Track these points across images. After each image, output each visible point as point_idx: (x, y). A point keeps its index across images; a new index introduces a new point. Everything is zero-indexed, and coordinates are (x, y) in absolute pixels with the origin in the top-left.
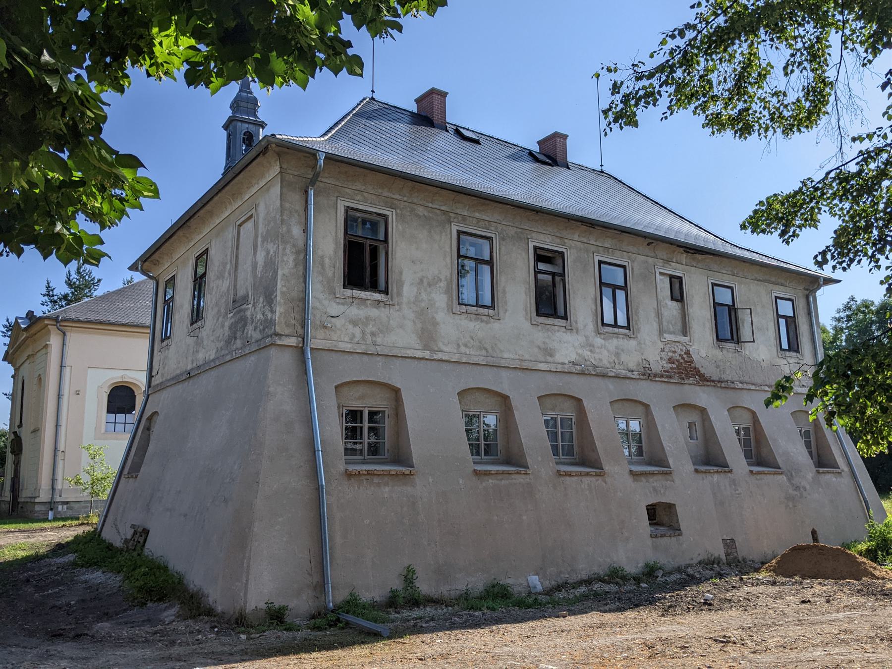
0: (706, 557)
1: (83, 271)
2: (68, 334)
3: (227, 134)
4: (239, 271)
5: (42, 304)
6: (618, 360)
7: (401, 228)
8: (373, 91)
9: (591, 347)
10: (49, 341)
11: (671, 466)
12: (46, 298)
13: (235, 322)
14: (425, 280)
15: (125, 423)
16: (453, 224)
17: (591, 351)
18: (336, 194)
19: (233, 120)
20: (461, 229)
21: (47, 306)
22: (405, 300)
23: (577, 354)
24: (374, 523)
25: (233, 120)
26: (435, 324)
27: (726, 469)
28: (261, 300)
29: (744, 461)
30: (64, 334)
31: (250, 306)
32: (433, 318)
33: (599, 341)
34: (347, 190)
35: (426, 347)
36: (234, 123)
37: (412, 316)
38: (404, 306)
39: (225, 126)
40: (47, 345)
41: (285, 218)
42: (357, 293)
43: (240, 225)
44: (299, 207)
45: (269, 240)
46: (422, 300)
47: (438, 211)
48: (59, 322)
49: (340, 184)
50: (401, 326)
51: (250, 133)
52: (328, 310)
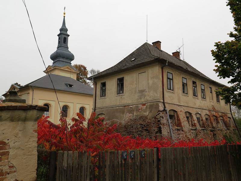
35: (179, 102)
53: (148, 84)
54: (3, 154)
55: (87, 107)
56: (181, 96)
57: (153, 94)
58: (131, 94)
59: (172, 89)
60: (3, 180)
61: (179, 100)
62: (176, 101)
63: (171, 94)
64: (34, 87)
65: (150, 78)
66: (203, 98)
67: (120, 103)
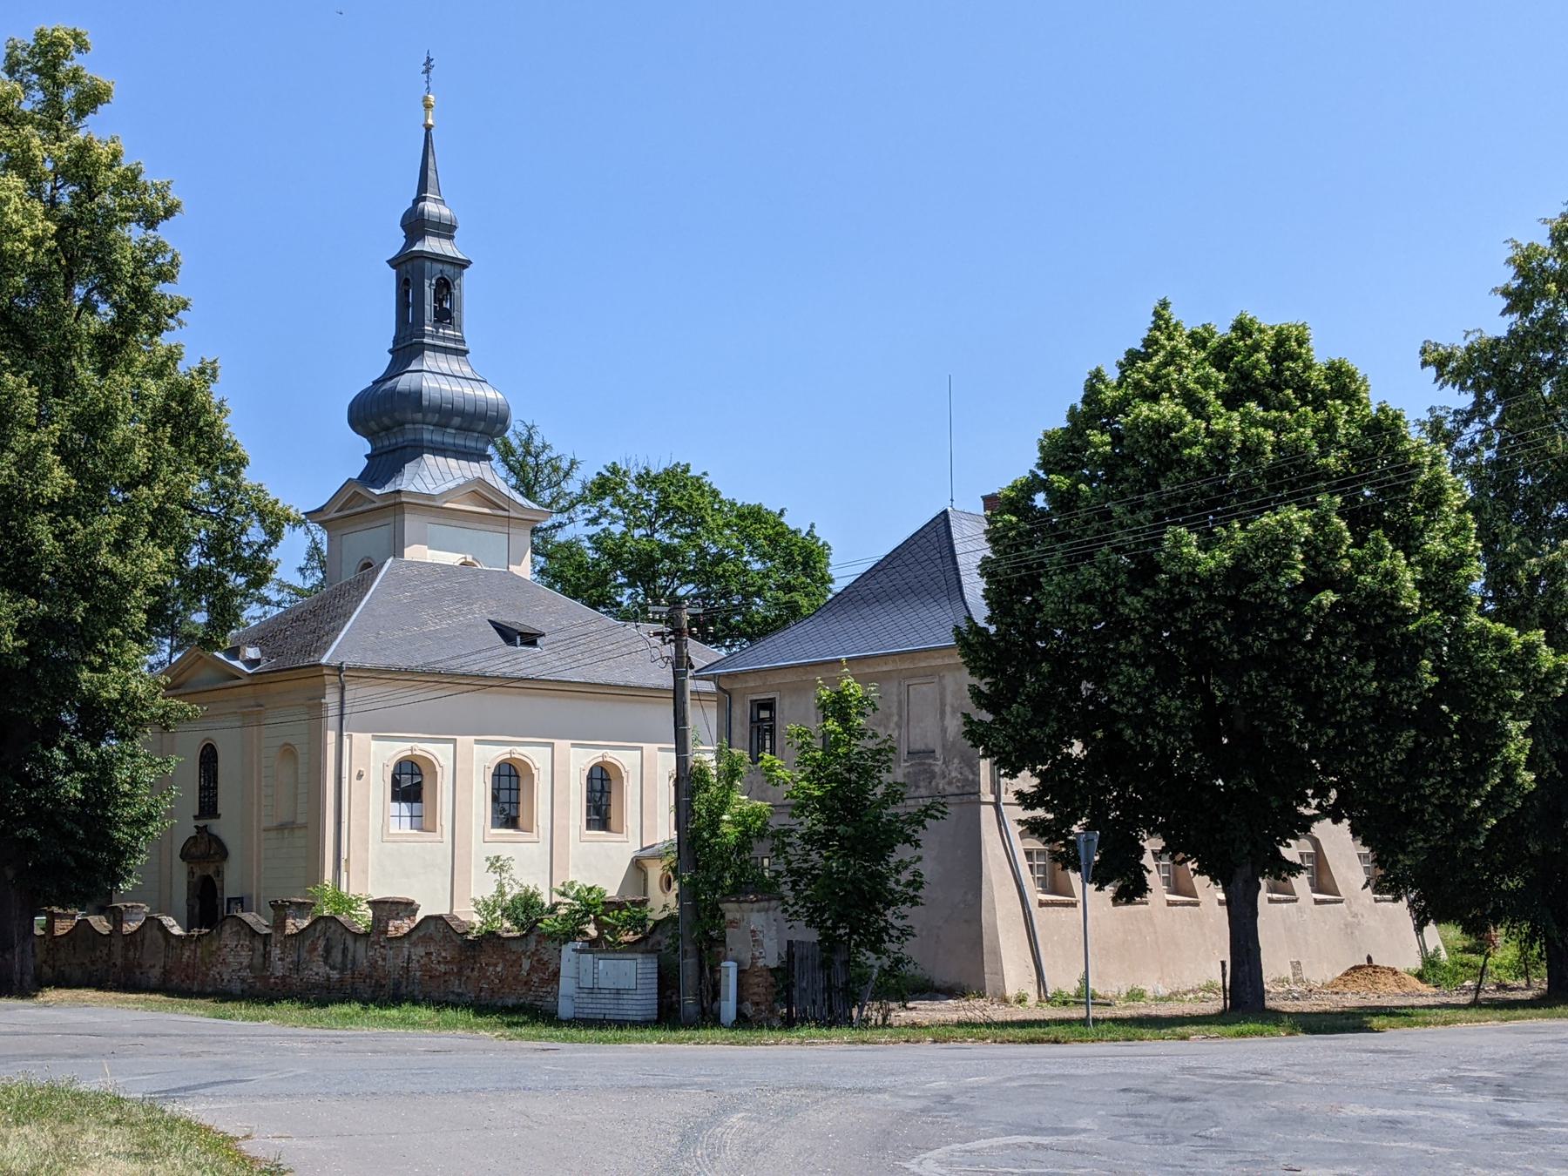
3: (398, 275)
28: (956, 761)
30: (343, 688)
53: (944, 730)
65: (948, 709)
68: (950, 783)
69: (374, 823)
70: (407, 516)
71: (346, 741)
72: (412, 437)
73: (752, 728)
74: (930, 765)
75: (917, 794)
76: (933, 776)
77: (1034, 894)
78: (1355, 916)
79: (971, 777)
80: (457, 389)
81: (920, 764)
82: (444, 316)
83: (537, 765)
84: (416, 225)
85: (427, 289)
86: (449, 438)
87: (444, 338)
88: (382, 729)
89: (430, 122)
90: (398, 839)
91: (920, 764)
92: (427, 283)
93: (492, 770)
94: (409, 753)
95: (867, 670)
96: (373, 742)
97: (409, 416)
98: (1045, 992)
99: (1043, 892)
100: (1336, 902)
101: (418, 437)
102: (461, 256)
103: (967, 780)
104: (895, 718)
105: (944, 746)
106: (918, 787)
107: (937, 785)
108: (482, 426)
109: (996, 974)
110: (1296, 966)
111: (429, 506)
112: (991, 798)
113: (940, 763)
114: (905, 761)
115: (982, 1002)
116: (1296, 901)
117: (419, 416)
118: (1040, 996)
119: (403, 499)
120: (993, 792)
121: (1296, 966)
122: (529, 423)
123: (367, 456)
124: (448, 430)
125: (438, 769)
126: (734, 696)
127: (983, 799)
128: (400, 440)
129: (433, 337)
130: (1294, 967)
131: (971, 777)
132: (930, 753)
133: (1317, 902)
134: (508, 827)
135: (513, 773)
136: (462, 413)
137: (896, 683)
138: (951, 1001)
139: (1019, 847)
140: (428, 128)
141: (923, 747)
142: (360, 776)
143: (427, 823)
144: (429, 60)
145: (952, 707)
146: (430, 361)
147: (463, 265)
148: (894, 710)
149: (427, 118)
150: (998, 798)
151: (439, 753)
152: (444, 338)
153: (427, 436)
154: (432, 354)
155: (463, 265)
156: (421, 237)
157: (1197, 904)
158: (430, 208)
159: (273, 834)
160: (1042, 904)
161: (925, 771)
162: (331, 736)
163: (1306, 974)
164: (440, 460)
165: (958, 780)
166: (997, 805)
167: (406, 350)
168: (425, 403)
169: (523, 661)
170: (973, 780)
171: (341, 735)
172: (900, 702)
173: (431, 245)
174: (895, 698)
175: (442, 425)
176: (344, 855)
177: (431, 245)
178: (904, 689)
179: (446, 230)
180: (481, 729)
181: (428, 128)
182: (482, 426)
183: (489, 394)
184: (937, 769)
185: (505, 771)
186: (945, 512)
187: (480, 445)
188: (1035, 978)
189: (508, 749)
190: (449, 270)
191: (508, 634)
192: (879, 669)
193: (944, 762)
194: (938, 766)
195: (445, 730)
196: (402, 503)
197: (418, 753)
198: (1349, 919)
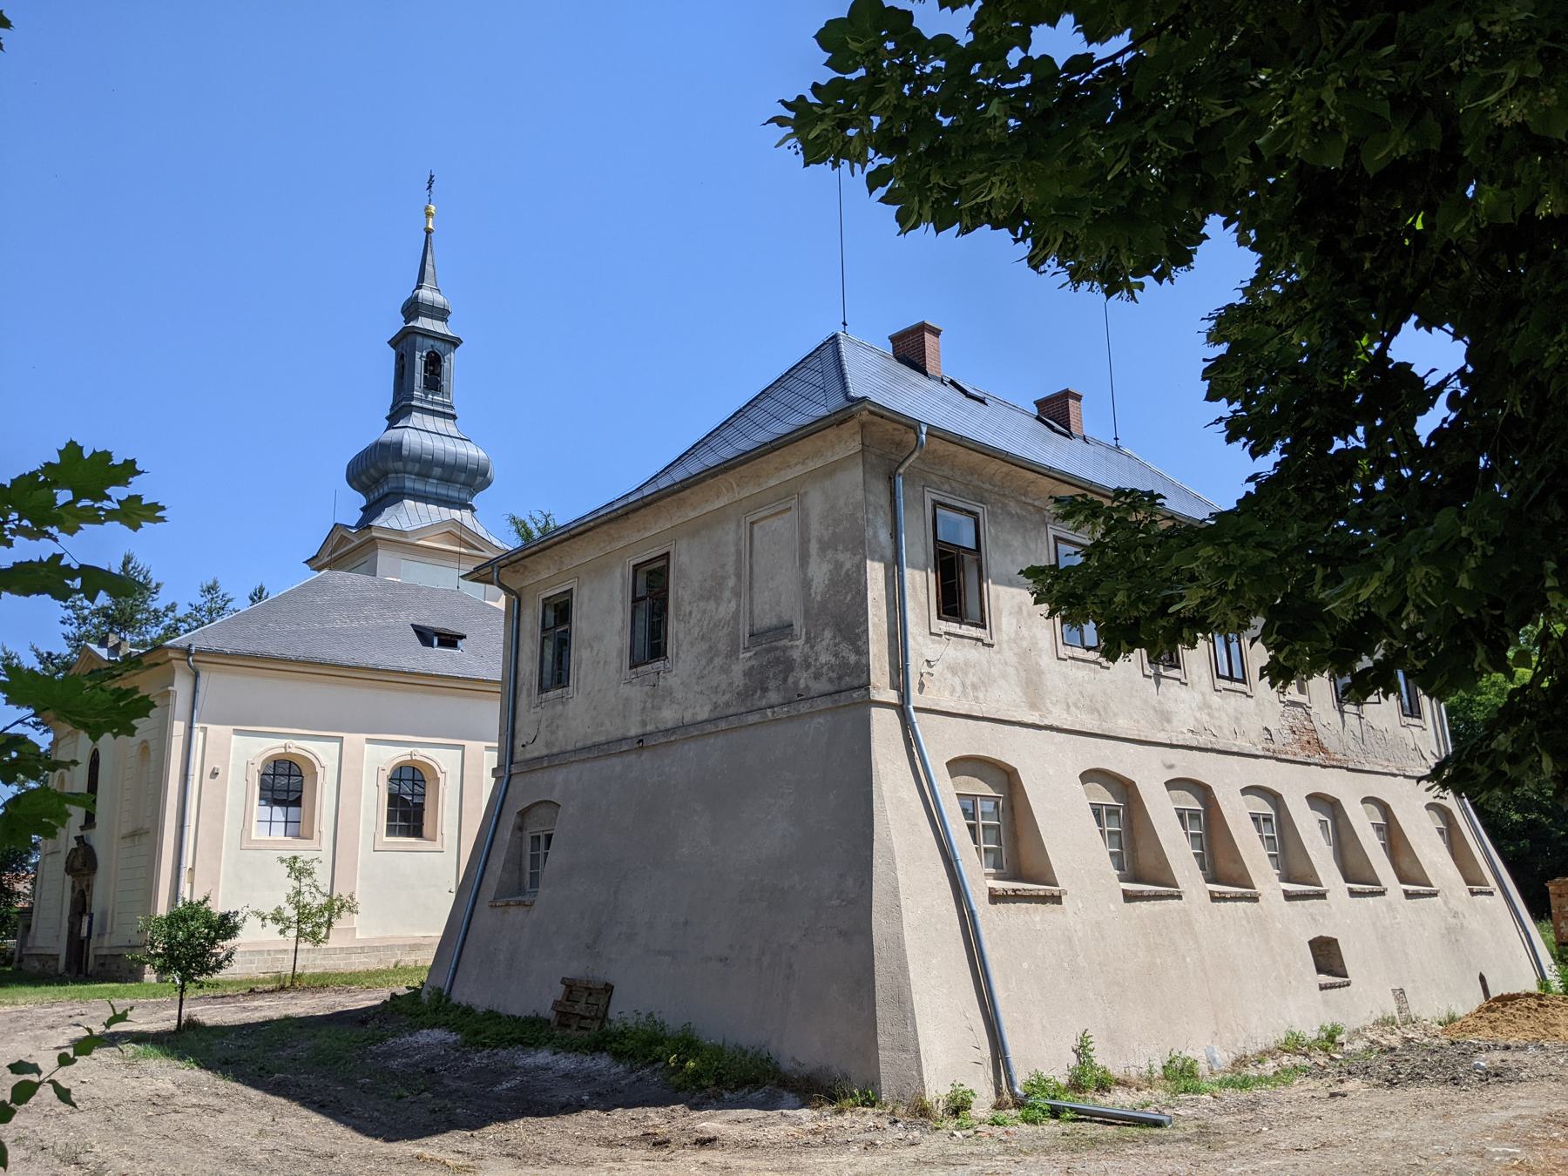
0: (1380, 1017)
1: (133, 568)
2: (202, 674)
3: (397, 354)
4: (755, 590)
5: (62, 622)
6: (1239, 727)
7: (993, 531)
8: (845, 324)
9: (1206, 706)
10: (173, 685)
11: (1323, 883)
12: (70, 612)
13: (761, 666)
14: (1024, 608)
15: (271, 821)
16: (1049, 526)
17: (1209, 715)
18: (922, 484)
19: (409, 333)
20: (1058, 534)
21: (71, 625)
22: (1005, 638)
23: (1196, 719)
24: (1033, 967)
25: (409, 333)
26: (1040, 673)
27: (1376, 888)
28: (828, 634)
29: (1274, 873)
30: (196, 676)
31: (800, 643)
32: (1037, 663)
33: (1216, 699)
34: (933, 477)
35: (1033, 706)
36: (410, 338)
37: (1013, 660)
38: (1005, 646)
39: (393, 343)
40: (169, 692)
41: (870, 516)
42: (953, 627)
43: (752, 523)
44: (884, 500)
45: (841, 548)
46: (1023, 638)
47: (1030, 508)
48: (191, 655)
49: (926, 469)
50: (1004, 676)
51: (436, 354)
52: (924, 650)
53: (806, 584)
54: (1564, 944)
55: (442, 760)
56: (1047, 661)
57: (836, 655)
58: (711, 660)
59: (1237, 674)
60: (104, 1174)
61: (1033, 685)
62: (1005, 699)
63: (953, 652)
64: (199, 652)
65: (814, 547)
66: (1231, 678)
67: (644, 723)
68: (817, 676)
69: (230, 827)
70: (380, 551)
71: (198, 736)
72: (394, 485)
73: (543, 639)
74: (785, 649)
75: (764, 703)
76: (788, 666)
77: (979, 879)
78: (1456, 915)
79: (853, 658)
80: (441, 445)
81: (768, 651)
82: (434, 383)
83: (444, 769)
84: (413, 308)
85: (417, 359)
86: (431, 487)
87: (432, 403)
88: (245, 720)
89: (430, 226)
90: (262, 846)
91: (768, 651)
92: (418, 355)
93: (388, 772)
94: (283, 751)
95: (692, 515)
96: (234, 737)
97: (390, 465)
98: (1011, 1082)
99: (997, 877)
100: (1372, 894)
101: (401, 485)
102: (450, 334)
103: (844, 664)
104: (731, 582)
105: (807, 613)
106: (765, 690)
107: (796, 683)
108: (463, 477)
109: (904, 1049)
110: (1400, 994)
111: (403, 544)
112: (892, 696)
113: (800, 643)
114: (747, 649)
115: (869, 1117)
116: (1382, 893)
117: (399, 465)
118: (998, 1093)
119: (374, 534)
120: (894, 686)
121: (1400, 994)
122: (546, 513)
123: (362, 509)
124: (431, 480)
125: (318, 769)
126: (526, 599)
127: (876, 695)
128: (381, 491)
129: (421, 400)
130: (1397, 998)
131: (853, 658)
132: (785, 629)
133: (1289, 896)
134: (408, 835)
135: (417, 776)
136: (442, 464)
137: (733, 526)
138: (805, 1113)
139: (947, 789)
140: (428, 232)
141: (775, 621)
142: (214, 774)
143: (304, 829)
144: (432, 177)
145: (820, 541)
146: (416, 419)
147: (455, 343)
148: (730, 569)
149: (428, 223)
150: (904, 696)
151: (322, 753)
152: (432, 403)
153: (408, 484)
154: (419, 415)
155: (455, 343)
156: (416, 318)
157: (1254, 899)
158: (426, 294)
159: (128, 840)
160: (995, 898)
161: (778, 661)
162: (179, 728)
163: (1414, 1010)
164: (420, 505)
165: (831, 668)
166: (902, 710)
167: (398, 413)
168: (405, 452)
169: (438, 659)
170: (857, 663)
171: (191, 728)
172: (739, 553)
173: (424, 323)
174: (732, 549)
175: (424, 475)
176: (187, 862)
177: (424, 323)
178: (744, 531)
179: (441, 314)
180: (371, 726)
181: (428, 232)
182: (463, 477)
183: (470, 452)
184: (796, 655)
185: (407, 775)
186: (835, 337)
187: (463, 496)
188: (986, 1052)
189: (408, 750)
190: (439, 346)
191: (425, 635)
192: (709, 507)
193: (808, 640)
194: (797, 648)
195: (332, 725)
196: (374, 539)
197: (294, 750)
198: (1450, 920)
